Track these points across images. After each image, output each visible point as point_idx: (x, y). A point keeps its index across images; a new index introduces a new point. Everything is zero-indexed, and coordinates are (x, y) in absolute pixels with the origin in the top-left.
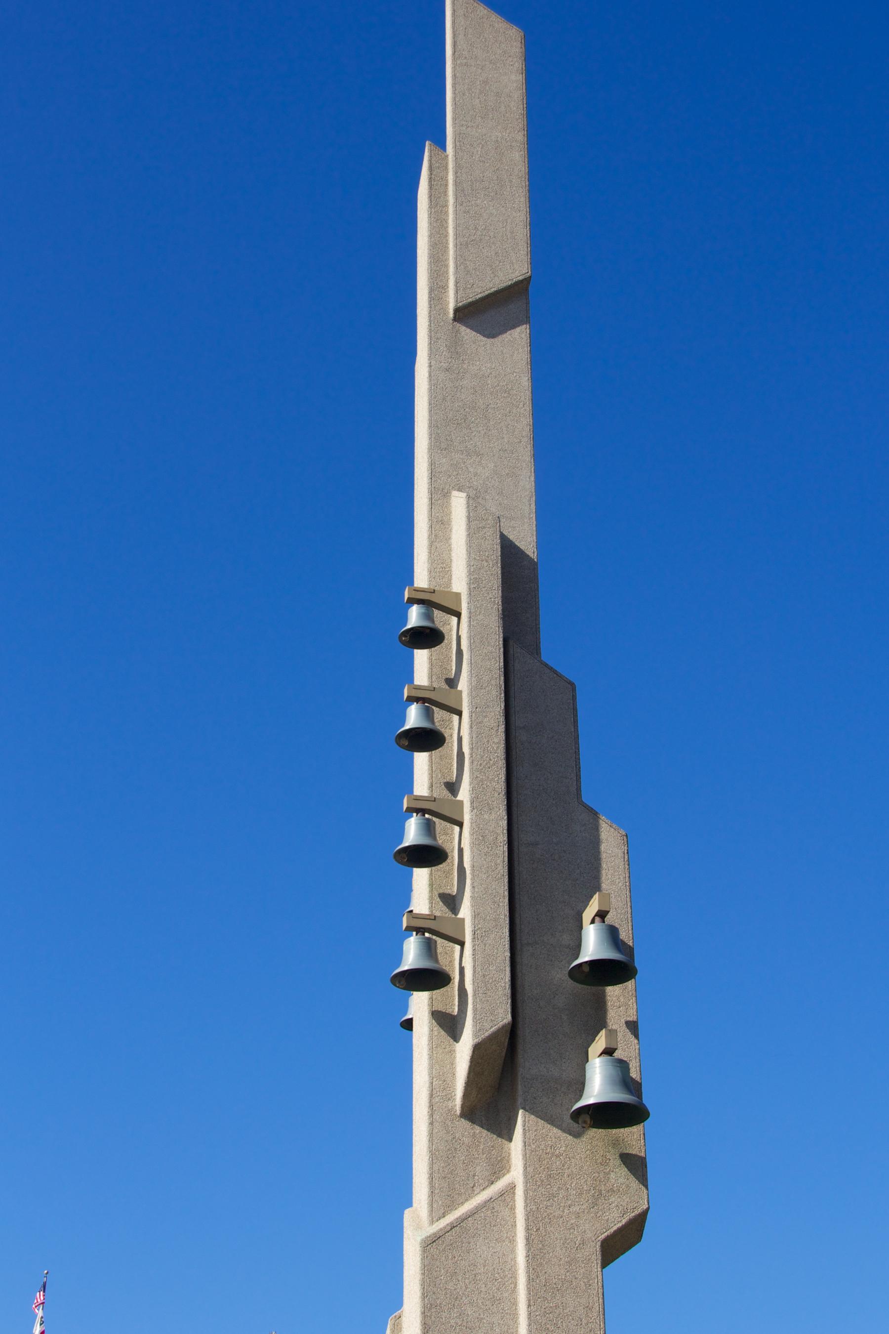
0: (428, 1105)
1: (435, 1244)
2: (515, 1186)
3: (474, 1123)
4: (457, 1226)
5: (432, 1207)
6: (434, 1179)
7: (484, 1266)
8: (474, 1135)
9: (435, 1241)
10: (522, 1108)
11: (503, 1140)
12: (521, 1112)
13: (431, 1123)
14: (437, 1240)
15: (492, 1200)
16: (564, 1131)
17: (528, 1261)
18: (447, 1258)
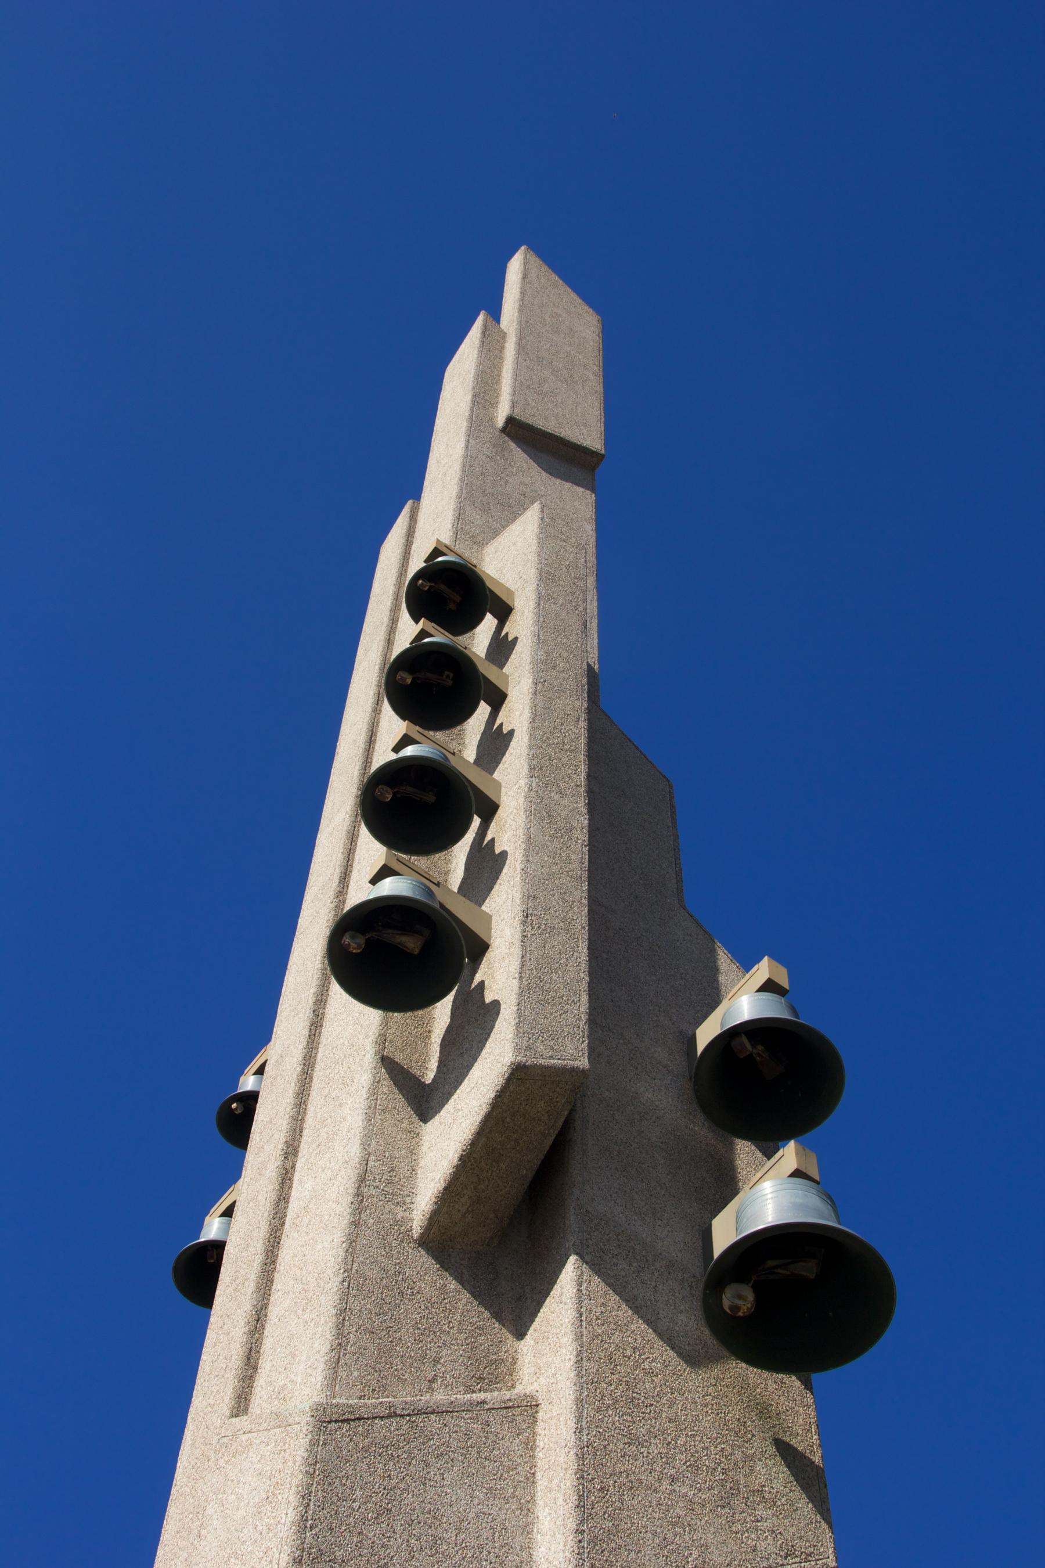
0: (352, 1191)
1: (346, 1427)
2: (537, 1406)
3: (446, 1270)
4: (402, 1416)
5: (336, 1372)
6: (347, 1323)
7: (459, 1531)
8: (443, 1289)
9: (347, 1421)
10: (577, 1254)
11: (504, 1330)
12: (573, 1259)
13: (356, 1224)
14: (354, 1420)
15: (487, 1407)
16: (660, 1335)
17: (580, 1541)
18: (371, 1469)
